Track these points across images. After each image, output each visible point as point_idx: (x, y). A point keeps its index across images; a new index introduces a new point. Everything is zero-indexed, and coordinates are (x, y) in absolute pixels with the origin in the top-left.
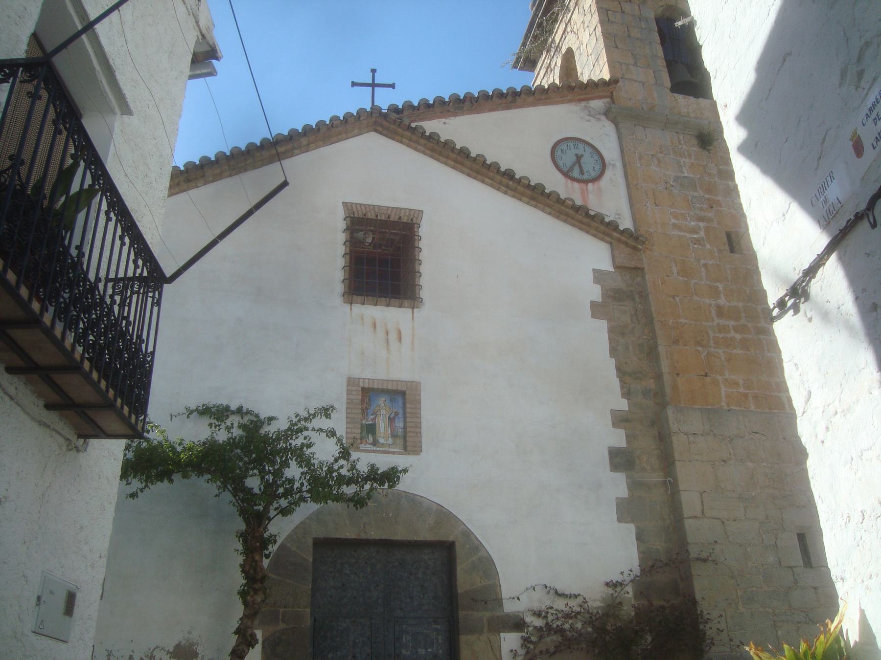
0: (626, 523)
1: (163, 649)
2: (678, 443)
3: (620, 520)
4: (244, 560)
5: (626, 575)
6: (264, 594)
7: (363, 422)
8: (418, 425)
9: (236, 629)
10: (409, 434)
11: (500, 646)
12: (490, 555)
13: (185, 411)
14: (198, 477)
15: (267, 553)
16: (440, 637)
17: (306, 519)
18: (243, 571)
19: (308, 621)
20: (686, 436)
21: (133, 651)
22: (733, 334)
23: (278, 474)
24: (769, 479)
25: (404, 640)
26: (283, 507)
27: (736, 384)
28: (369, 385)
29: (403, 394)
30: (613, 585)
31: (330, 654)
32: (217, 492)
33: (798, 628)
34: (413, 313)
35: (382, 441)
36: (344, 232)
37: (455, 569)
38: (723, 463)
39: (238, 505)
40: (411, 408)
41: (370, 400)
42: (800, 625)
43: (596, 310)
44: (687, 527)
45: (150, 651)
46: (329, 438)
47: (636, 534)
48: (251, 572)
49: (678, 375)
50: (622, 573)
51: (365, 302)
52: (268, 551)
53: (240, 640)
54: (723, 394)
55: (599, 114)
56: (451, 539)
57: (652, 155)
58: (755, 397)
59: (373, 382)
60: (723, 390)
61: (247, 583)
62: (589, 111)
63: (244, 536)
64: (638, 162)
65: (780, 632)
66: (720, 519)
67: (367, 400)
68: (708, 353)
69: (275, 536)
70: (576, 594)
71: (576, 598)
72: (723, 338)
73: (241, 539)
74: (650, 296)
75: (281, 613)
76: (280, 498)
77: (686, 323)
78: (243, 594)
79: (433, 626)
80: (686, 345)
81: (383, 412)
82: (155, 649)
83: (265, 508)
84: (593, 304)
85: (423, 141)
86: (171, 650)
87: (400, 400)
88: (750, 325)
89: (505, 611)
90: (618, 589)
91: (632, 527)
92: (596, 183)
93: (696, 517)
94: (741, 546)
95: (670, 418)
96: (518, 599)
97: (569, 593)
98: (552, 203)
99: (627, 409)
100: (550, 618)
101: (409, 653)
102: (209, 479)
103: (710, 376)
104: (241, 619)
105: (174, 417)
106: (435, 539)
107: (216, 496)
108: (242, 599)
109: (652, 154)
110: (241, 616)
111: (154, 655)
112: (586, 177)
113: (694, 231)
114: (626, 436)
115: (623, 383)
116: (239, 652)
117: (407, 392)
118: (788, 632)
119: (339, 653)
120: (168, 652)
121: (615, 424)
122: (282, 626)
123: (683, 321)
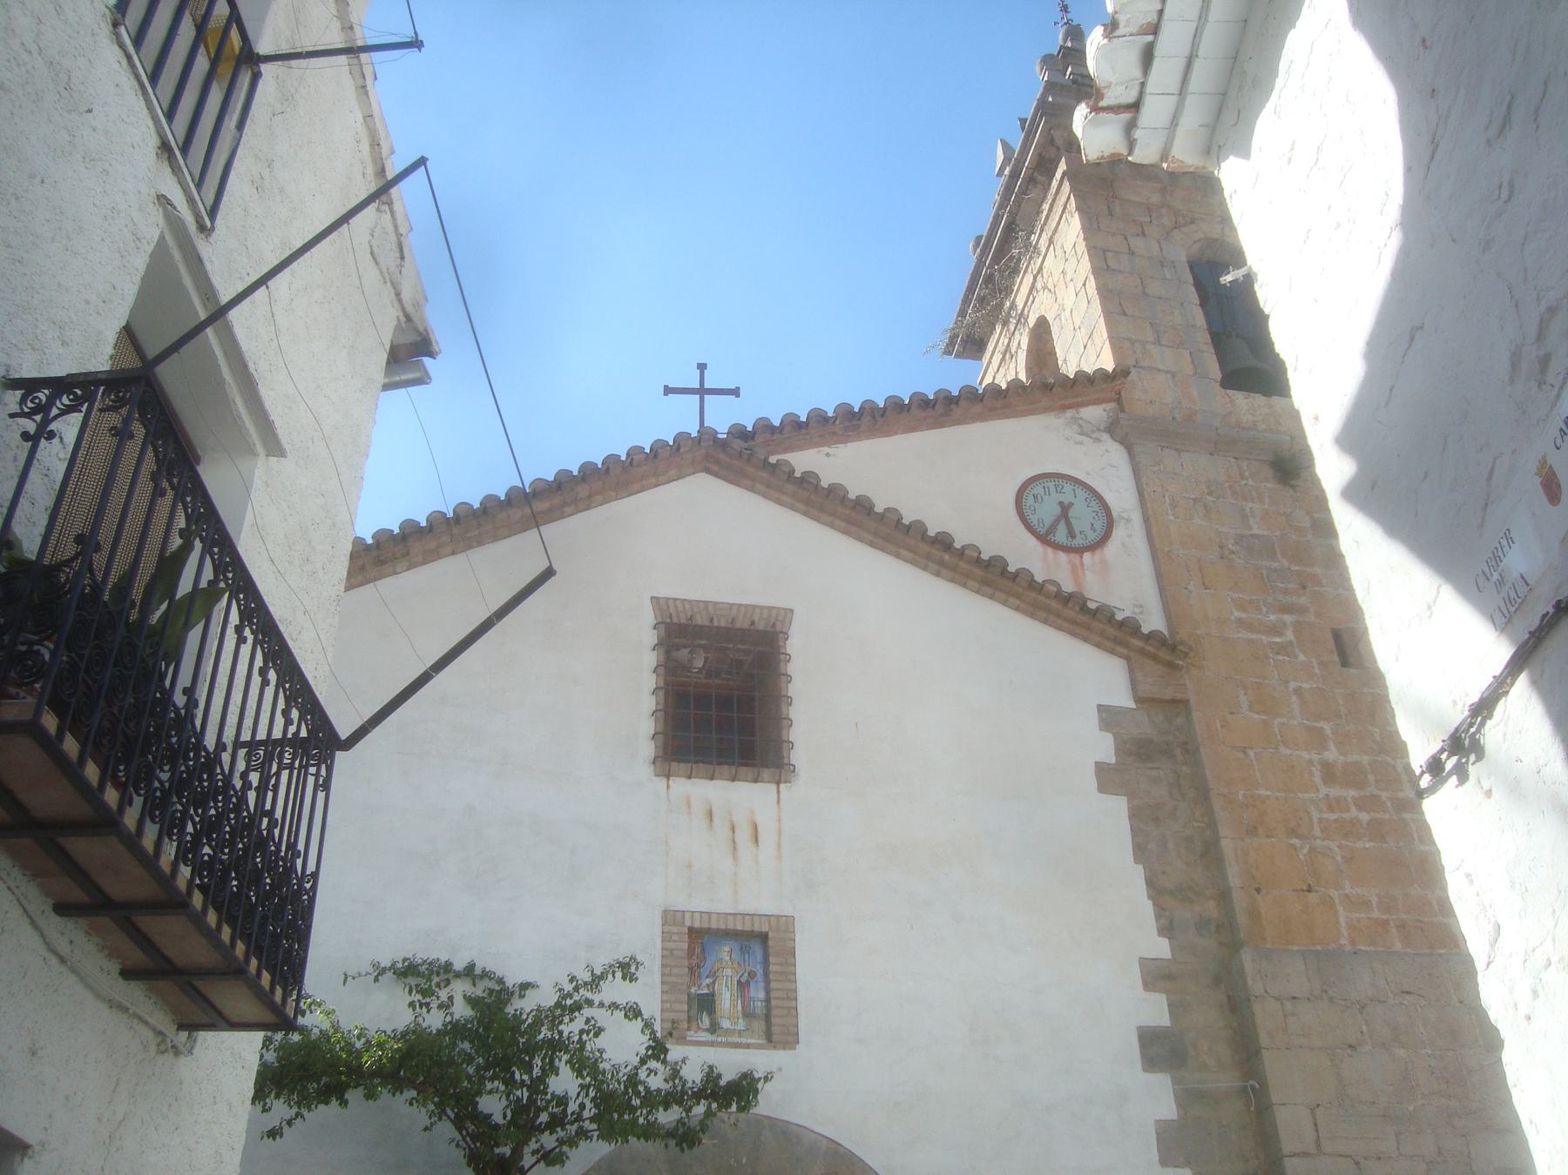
0: (1176, 1167)
2: (1265, 1016)
7: (693, 990)
8: (791, 995)
10: (775, 1012)
17: (588, 1171)
22: (1354, 812)
23: (538, 1086)
27: (1366, 904)
29: (763, 938)
34: (778, 792)
35: (726, 1024)
36: (654, 649)
38: (1349, 1051)
39: (465, 1145)
40: (779, 964)
41: (703, 950)
43: (1108, 778)
49: (1258, 890)
51: (694, 774)
54: (1342, 921)
55: (1099, 430)
57: (1195, 500)
62: (1080, 426)
64: (1169, 512)
67: (698, 950)
68: (1311, 848)
72: (1336, 821)
74: (1202, 750)
76: (542, 1132)
77: (1268, 796)
80: (1273, 837)
81: (729, 972)
84: (1100, 768)
85: (789, 487)
88: (1384, 795)
92: (1098, 553)
93: (1306, 1154)
98: (1020, 590)
99: (1170, 957)
102: (413, 1099)
103: (1316, 891)
105: (349, 979)
107: (426, 1129)
109: (1194, 496)
112: (1078, 542)
113: (1275, 630)
114: (1169, 1005)
117: (770, 935)
121: (1147, 986)
123: (1263, 792)
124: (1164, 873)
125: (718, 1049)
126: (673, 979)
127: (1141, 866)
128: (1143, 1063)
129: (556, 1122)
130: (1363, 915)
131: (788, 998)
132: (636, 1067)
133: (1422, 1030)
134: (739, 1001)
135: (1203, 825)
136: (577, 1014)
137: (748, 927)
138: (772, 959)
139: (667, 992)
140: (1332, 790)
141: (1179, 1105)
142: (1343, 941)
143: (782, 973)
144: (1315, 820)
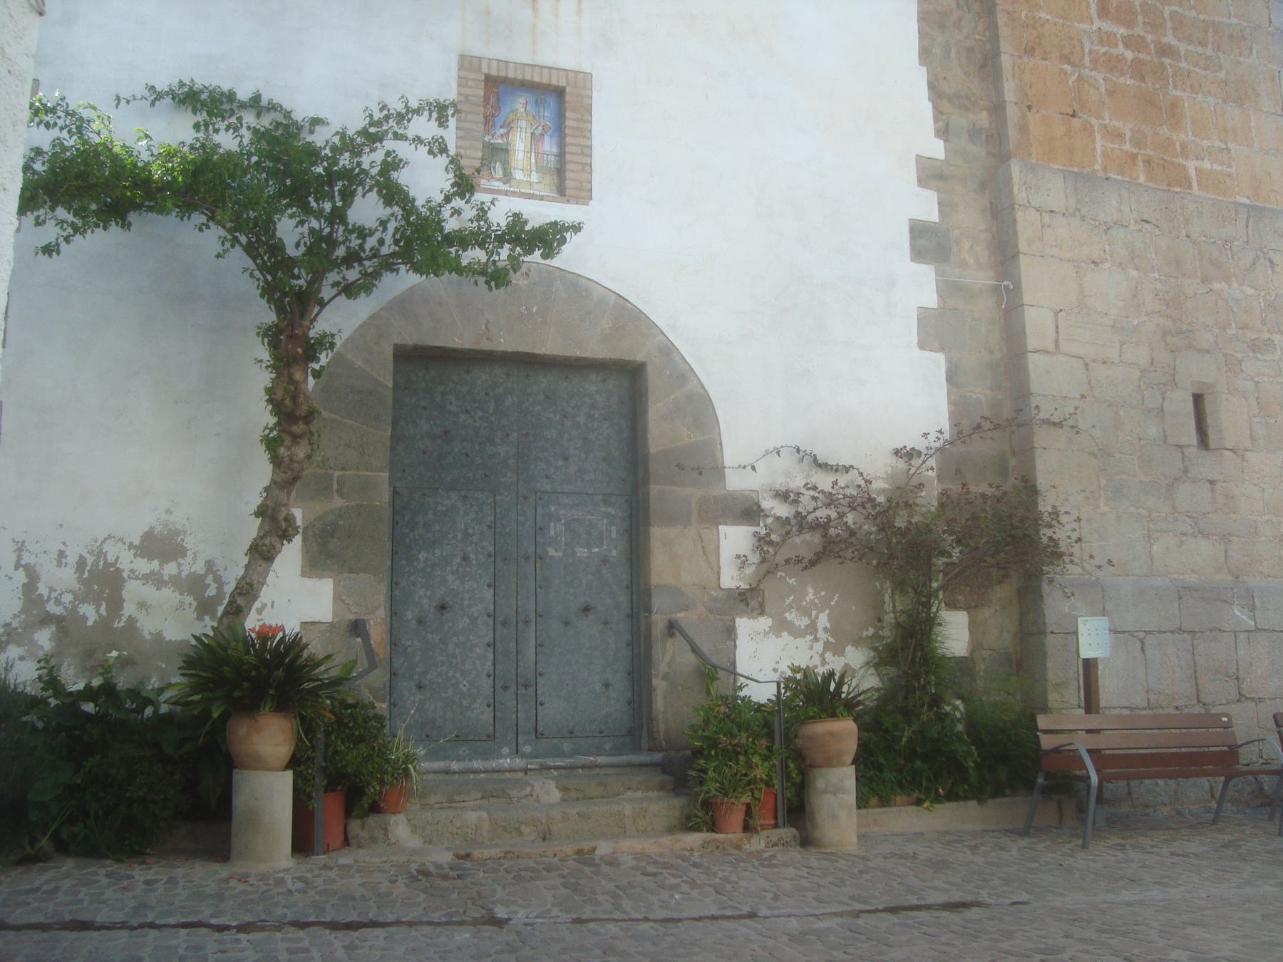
0: (931, 351)
1: (121, 540)
2: (1026, 223)
3: (922, 346)
4: (273, 380)
5: (932, 438)
6: (311, 444)
7: (486, 139)
8: (587, 151)
9: (258, 507)
10: (569, 167)
11: (718, 547)
12: (706, 391)
13: (146, 94)
14: (182, 219)
15: (317, 367)
16: (614, 528)
17: (380, 310)
18: (270, 401)
19: (385, 496)
20: (1038, 213)
21: (64, 544)
22: (1121, 49)
23: (338, 216)
24: (1160, 300)
25: (552, 533)
26: (349, 282)
27: (1120, 136)
28: (498, 71)
29: (560, 93)
30: (906, 454)
31: (422, 553)
32: (219, 249)
33: (1182, 542)
35: (518, 175)
37: (645, 412)
38: (1092, 266)
40: (574, 120)
41: (498, 100)
42: (1184, 538)
44: (1031, 366)
45: (98, 544)
46: (435, 156)
47: (947, 372)
48: (287, 402)
49: (1029, 108)
50: (925, 435)
52: (319, 365)
53: (267, 527)
54: (1099, 150)
56: (639, 358)
58: (1148, 162)
59: (507, 68)
60: (1099, 143)
61: (279, 423)
63: (273, 336)
65: (1155, 547)
66: (1081, 358)
67: (493, 100)
68: (1079, 76)
69: (333, 336)
70: (847, 465)
71: (847, 472)
72: (1105, 54)
73: (266, 340)
75: (335, 479)
77: (1047, 20)
78: (271, 445)
79: (603, 509)
80: (1047, 59)
82: (105, 539)
83: (310, 283)
86: (137, 542)
87: (552, 102)
88: (1150, 38)
89: (728, 489)
90: (916, 462)
91: (941, 358)
93: (1046, 352)
94: (1110, 405)
95: (1014, 180)
96: (753, 468)
97: (835, 464)
99: (943, 158)
100: (805, 499)
101: (561, 554)
102: (203, 224)
103: (1080, 117)
104: (266, 489)
106: (612, 357)
107: (219, 256)
108: (270, 452)
110: (266, 482)
111: (104, 551)
114: (939, 203)
115: (938, 112)
116: (265, 548)
117: (568, 90)
118: (1167, 549)
119: (438, 551)
120: (131, 546)
121: (922, 182)
122: (338, 502)
123: (1043, 15)
124: (945, 78)
125: (512, 198)
126: (468, 126)
127: (925, 69)
128: (911, 253)
129: (352, 258)
130: (1117, 146)
131: (583, 154)
132: (439, 204)
133: (1153, 256)
134: (533, 154)
135: (984, 39)
136: (378, 144)
137: (545, 81)
138: (568, 114)
139: (461, 138)
140: (1105, 25)
141: (940, 296)
142: (1097, 167)
143: (578, 129)
144: (1087, 51)
